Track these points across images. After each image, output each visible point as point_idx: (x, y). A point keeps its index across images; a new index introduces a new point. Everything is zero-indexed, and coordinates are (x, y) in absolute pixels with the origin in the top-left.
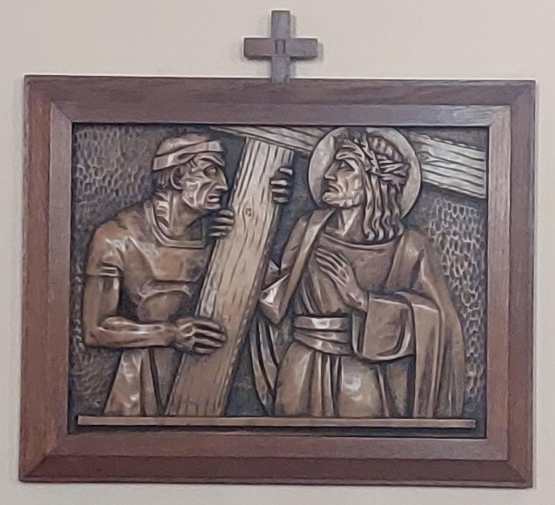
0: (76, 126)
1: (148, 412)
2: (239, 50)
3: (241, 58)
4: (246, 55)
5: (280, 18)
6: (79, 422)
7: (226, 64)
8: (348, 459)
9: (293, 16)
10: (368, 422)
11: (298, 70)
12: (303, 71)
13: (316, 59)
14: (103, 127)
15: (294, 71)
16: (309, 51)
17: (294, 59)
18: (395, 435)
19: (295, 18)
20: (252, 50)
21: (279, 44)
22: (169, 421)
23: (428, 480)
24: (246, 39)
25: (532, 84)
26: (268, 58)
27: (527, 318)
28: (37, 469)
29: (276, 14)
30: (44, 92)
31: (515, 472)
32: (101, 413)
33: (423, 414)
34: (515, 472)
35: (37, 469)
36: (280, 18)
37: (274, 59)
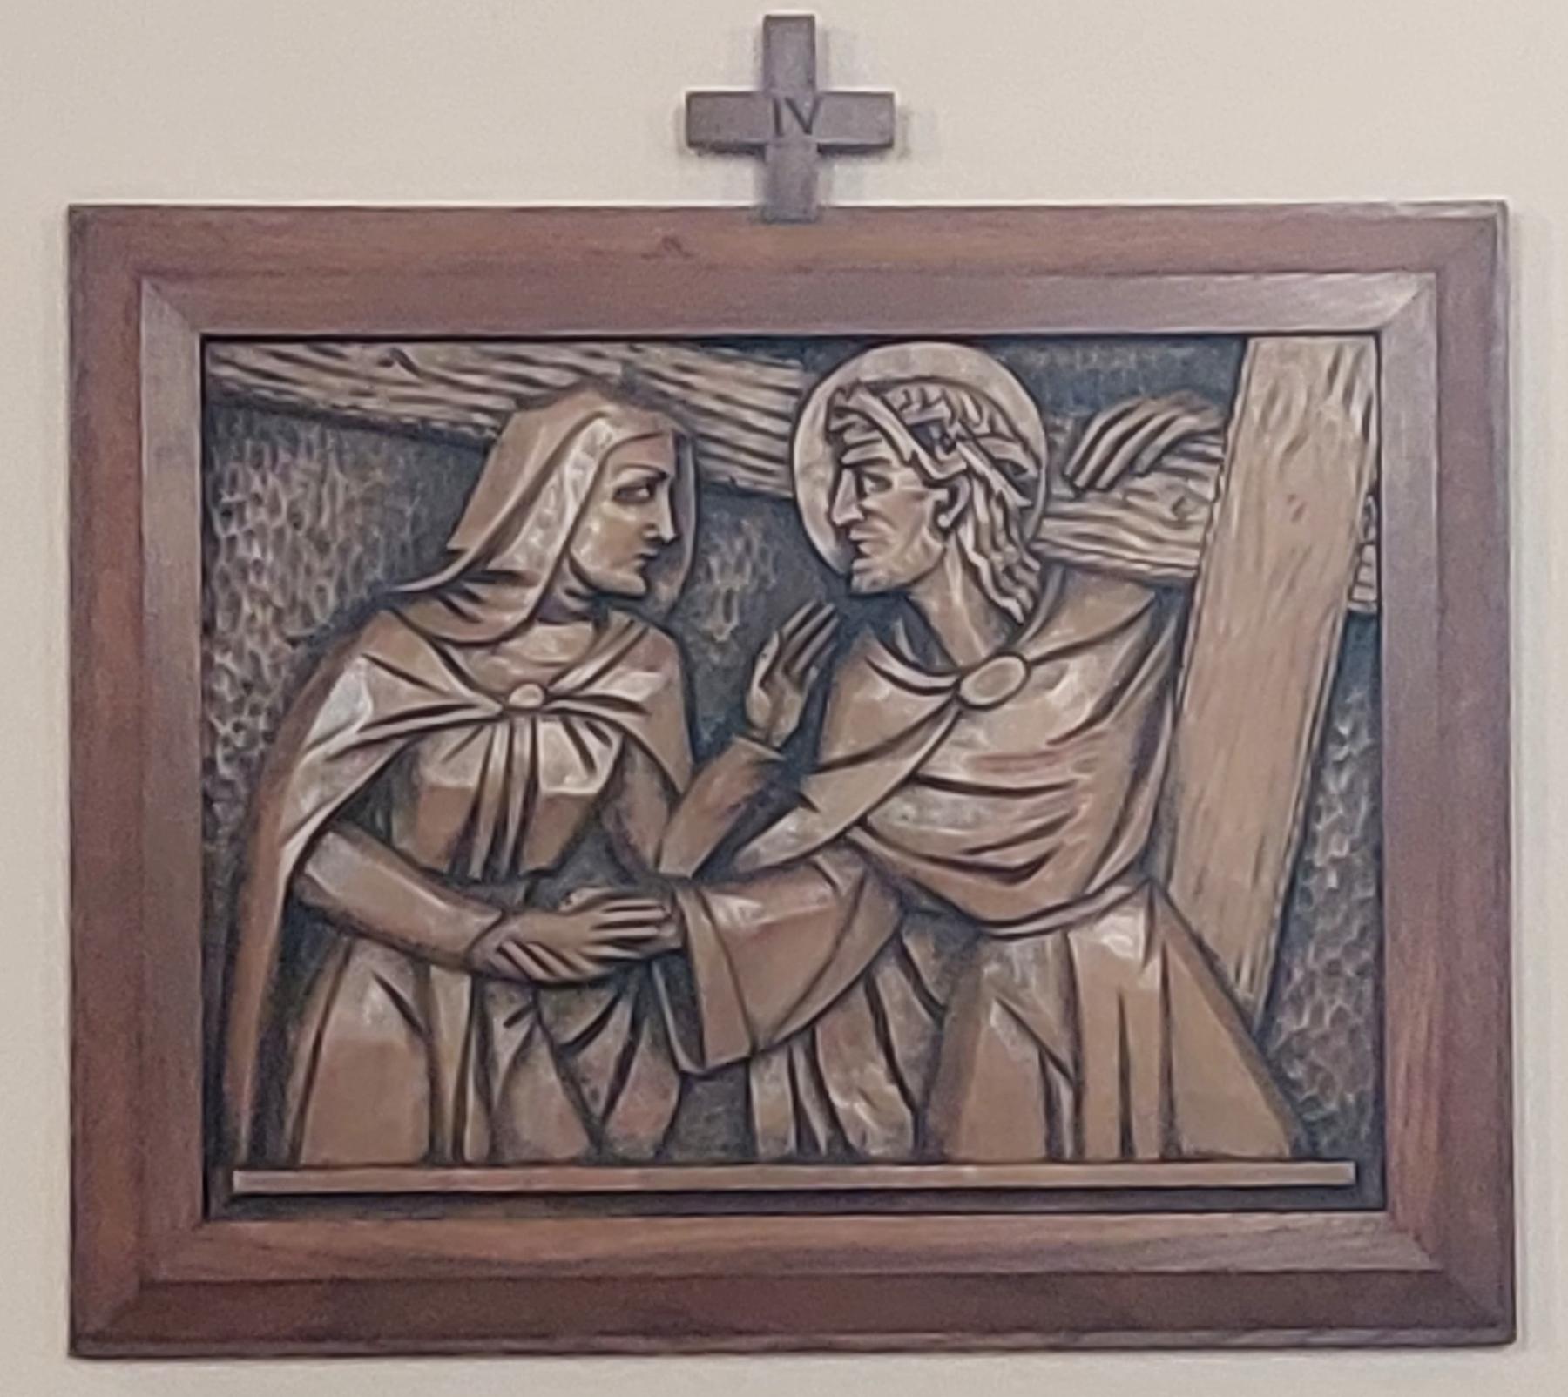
0: (207, 340)
1: (469, 1154)
2: (671, 128)
3: (681, 152)
5: (787, 37)
7: (636, 167)
8: (332, 1281)
9: (826, 34)
10: (1269, 1173)
11: (839, 184)
12: (858, 186)
13: (892, 154)
15: (829, 188)
16: (873, 132)
19: (826, 34)
20: (709, 127)
21: (782, 113)
23: (1331, 1327)
24: (692, 98)
25: (76, 216)
26: (755, 151)
30: (85, 225)
31: (1467, 1304)
32: (292, 1164)
33: (931, 1151)
34: (1467, 1304)
35: (92, 1338)
36: (787, 37)
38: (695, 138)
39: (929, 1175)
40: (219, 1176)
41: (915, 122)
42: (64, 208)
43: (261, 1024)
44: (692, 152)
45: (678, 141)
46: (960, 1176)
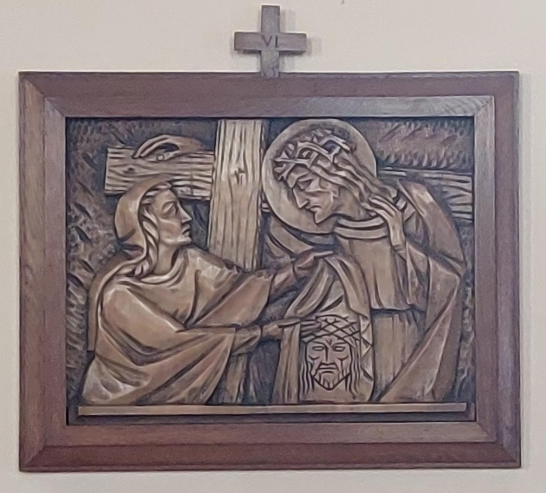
3: (232, 53)
4: (236, 49)
5: (271, 13)
6: (465, 404)
13: (305, 54)
14: (97, 123)
16: (299, 46)
17: (283, 53)
18: (389, 420)
19: (284, 14)
20: (242, 44)
21: (270, 37)
22: (270, 409)
24: (236, 34)
27: (178, 464)
28: (36, 458)
29: (265, 9)
35: (36, 458)
36: (271, 13)
37: (263, 53)
38: (238, 47)
39: (310, 409)
40: (72, 409)
41: (313, 43)
42: (16, 74)
43: (447, 270)
44: (236, 52)
45: (231, 49)
46: (334, 409)
